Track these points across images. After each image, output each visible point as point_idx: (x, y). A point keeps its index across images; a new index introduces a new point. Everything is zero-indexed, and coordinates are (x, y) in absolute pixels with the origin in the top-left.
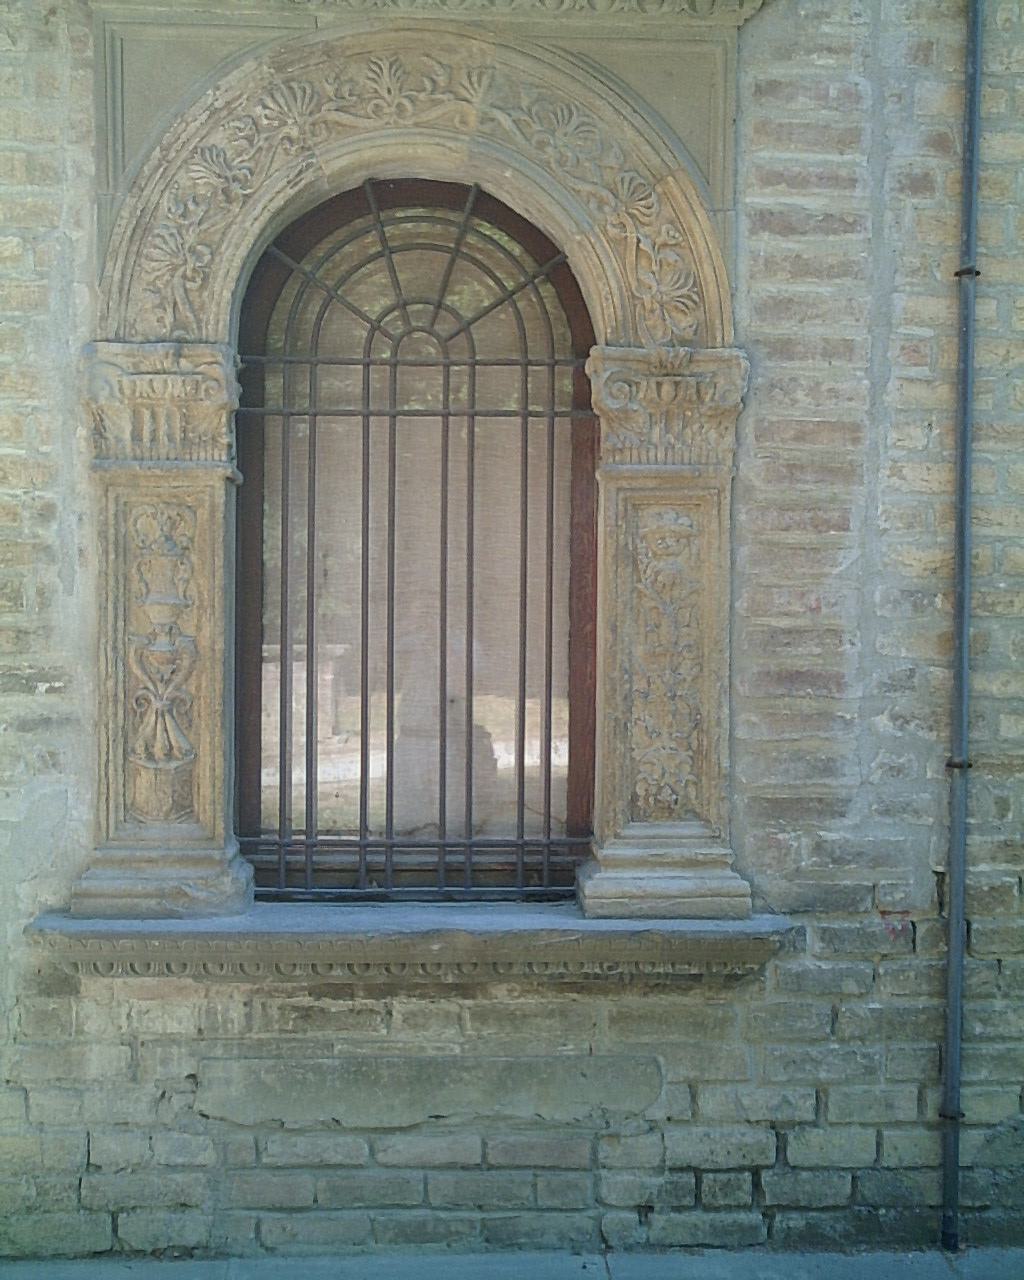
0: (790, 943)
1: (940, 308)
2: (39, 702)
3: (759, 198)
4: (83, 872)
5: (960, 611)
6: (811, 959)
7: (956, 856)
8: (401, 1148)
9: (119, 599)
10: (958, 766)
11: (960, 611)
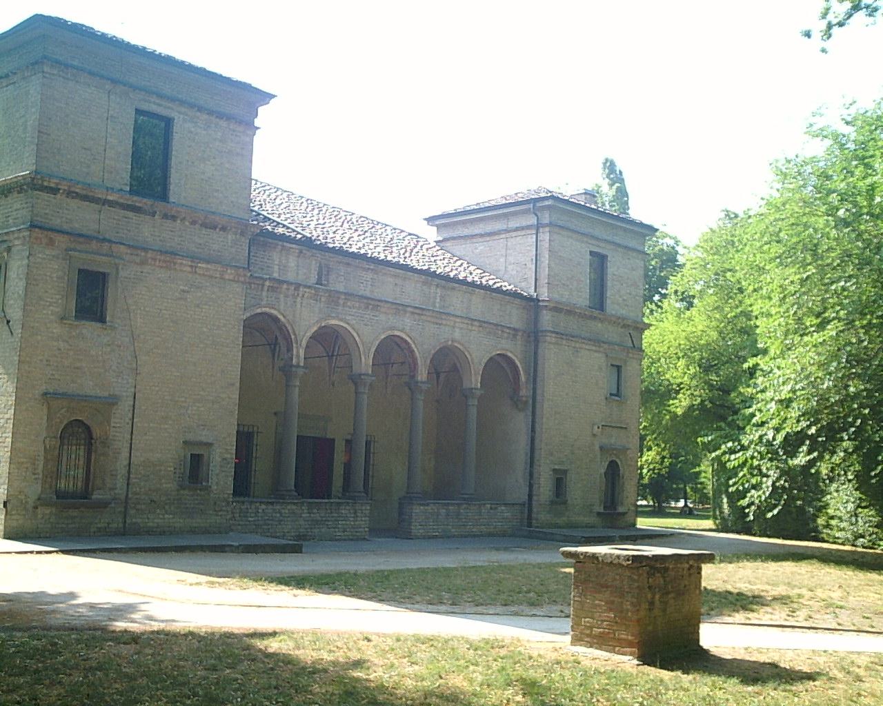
0: (110, 503)
1: (129, 437)
2: (37, 476)
3: (112, 425)
4: (40, 495)
5: (129, 468)
6: (113, 505)
7: (127, 495)
8: (70, 526)
9: (45, 465)
10: (128, 484)
11: (129, 468)
